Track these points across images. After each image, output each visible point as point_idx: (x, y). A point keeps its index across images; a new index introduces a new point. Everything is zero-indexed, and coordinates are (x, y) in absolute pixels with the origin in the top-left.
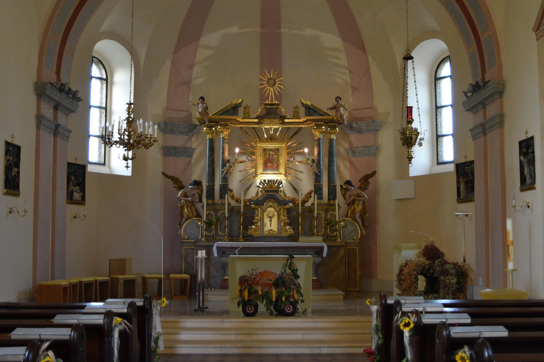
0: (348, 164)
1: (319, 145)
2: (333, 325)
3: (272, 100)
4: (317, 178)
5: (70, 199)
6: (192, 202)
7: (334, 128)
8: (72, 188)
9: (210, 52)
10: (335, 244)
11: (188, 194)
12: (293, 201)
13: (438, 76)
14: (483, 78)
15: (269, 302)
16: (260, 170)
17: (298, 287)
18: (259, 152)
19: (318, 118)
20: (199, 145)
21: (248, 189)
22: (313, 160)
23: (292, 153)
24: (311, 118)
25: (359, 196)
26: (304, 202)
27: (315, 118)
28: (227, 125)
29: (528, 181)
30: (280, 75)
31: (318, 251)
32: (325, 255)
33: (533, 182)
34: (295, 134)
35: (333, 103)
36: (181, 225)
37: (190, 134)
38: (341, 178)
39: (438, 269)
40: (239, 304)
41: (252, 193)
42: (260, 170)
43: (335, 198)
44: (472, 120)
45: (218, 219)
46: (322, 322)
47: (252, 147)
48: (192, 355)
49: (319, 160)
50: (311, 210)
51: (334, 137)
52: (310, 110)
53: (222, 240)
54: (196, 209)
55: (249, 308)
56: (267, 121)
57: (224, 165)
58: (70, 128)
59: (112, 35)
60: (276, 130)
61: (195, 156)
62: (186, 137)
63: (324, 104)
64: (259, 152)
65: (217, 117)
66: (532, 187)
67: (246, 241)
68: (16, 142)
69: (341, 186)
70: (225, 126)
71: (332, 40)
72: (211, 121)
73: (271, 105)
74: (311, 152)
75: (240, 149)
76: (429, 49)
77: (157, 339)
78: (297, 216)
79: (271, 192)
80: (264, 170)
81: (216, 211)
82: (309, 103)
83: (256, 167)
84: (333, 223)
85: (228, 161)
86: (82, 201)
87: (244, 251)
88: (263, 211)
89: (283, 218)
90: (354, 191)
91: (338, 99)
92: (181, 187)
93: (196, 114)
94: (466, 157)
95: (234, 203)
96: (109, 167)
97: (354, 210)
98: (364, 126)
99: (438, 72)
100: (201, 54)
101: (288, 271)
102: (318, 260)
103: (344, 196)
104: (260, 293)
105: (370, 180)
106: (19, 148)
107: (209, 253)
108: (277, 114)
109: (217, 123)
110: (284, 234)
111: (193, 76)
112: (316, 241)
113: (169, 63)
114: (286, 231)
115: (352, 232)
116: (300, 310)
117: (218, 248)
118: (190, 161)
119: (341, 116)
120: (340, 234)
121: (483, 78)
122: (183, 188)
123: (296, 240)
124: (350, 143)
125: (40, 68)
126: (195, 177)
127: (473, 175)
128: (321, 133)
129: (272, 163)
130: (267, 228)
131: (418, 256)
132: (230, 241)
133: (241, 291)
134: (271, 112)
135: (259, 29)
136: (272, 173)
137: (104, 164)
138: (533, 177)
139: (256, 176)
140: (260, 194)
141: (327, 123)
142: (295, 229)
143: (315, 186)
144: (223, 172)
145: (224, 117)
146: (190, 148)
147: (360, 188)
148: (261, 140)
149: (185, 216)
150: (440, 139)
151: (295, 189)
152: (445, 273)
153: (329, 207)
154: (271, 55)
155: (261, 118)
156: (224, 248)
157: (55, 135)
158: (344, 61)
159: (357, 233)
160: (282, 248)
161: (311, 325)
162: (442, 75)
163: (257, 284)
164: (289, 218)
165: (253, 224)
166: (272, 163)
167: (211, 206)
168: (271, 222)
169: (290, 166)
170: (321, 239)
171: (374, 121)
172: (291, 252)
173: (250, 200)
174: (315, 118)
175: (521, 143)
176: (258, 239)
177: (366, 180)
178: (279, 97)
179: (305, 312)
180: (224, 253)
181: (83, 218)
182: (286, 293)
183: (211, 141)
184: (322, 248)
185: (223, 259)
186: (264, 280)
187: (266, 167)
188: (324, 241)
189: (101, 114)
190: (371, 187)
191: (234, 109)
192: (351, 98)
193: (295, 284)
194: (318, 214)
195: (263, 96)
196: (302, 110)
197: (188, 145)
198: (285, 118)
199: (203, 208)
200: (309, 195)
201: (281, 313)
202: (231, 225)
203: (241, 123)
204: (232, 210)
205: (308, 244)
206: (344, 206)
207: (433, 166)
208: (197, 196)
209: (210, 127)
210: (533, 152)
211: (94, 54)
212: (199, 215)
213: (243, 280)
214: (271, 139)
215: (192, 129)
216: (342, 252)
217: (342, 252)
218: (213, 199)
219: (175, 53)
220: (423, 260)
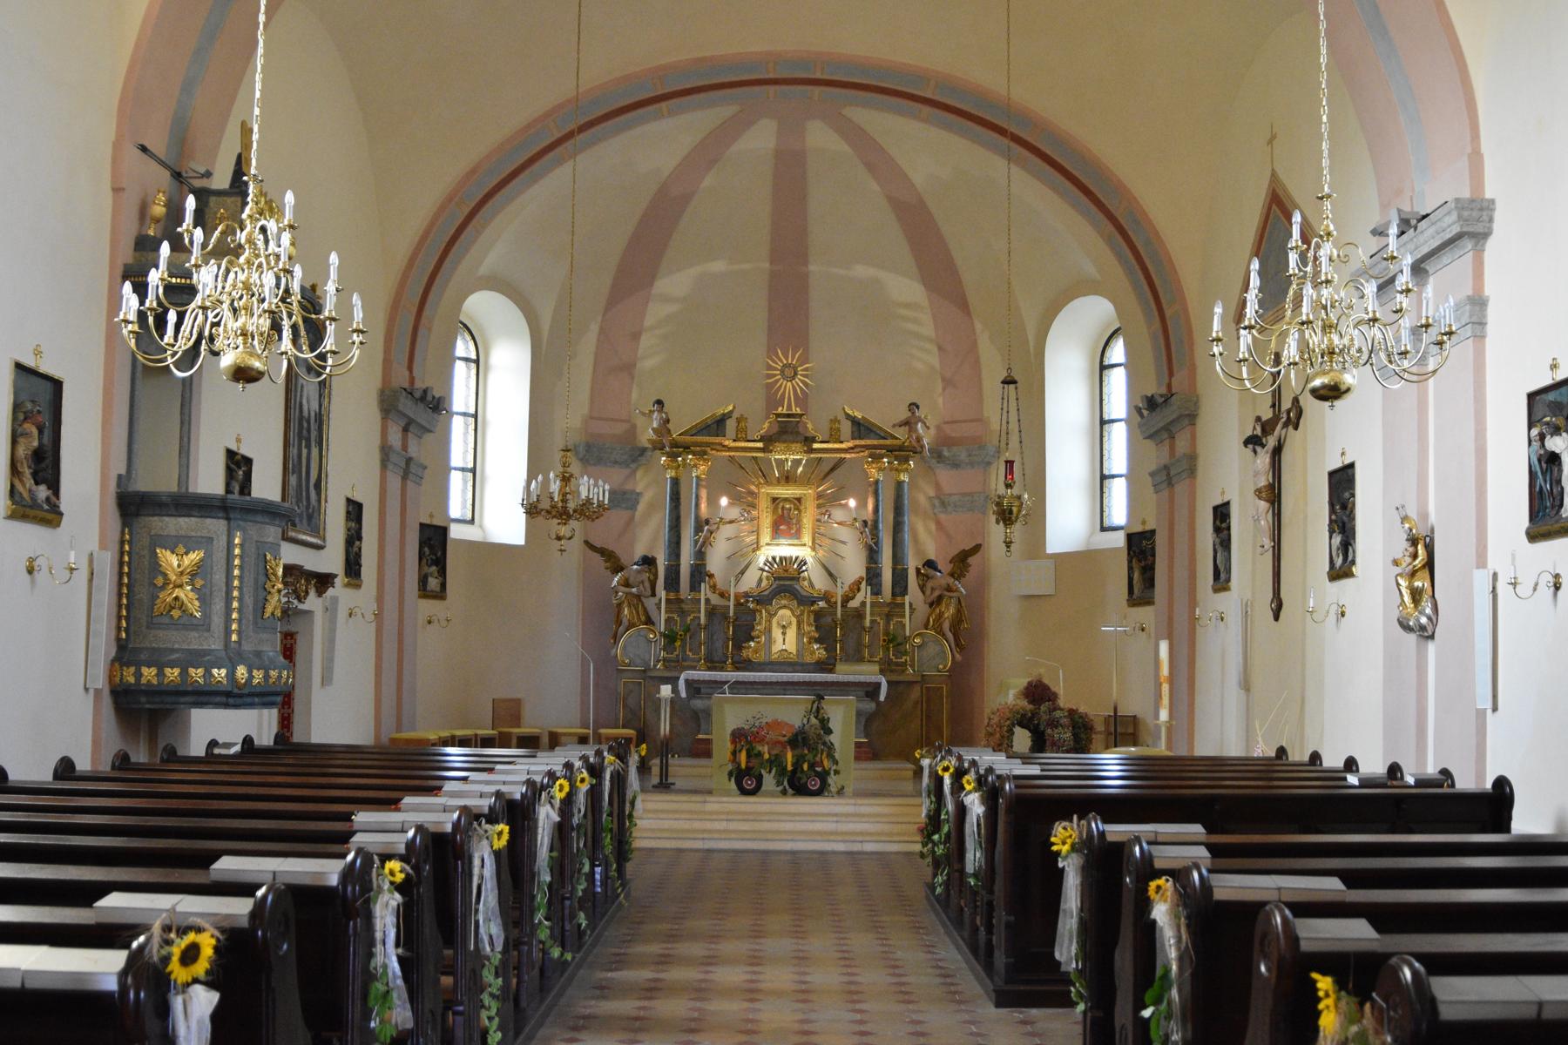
0: (933, 527)
1: (876, 493)
2: (886, 810)
3: (789, 407)
4: (873, 554)
5: (424, 592)
6: (638, 597)
7: (906, 460)
8: (426, 569)
9: (671, 308)
10: (901, 678)
11: (631, 581)
12: (826, 597)
13: (1106, 362)
14: (1169, 386)
15: (782, 771)
16: (766, 537)
17: (830, 748)
18: (764, 504)
19: (875, 442)
20: (651, 485)
21: (742, 572)
22: (865, 522)
23: (827, 503)
24: (862, 442)
25: (949, 589)
26: (847, 599)
27: (869, 442)
28: (705, 453)
29: (1223, 576)
30: (804, 359)
31: (871, 691)
32: (882, 698)
33: (1228, 580)
34: (832, 470)
35: (904, 414)
36: (616, 638)
37: (633, 466)
38: (919, 552)
39: (1045, 717)
40: (730, 774)
41: (749, 582)
42: (766, 537)
43: (904, 592)
44: (1155, 456)
45: (688, 630)
46: (868, 806)
47: (751, 493)
48: (658, 849)
49: (876, 522)
50: (859, 614)
51: (904, 477)
52: (861, 428)
53: (694, 668)
54: (645, 609)
55: (746, 781)
56: (780, 446)
57: (698, 529)
58: (426, 463)
59: (496, 283)
60: (797, 463)
61: (641, 507)
62: (626, 471)
63: (886, 415)
64: (764, 504)
65: (688, 439)
66: (1225, 588)
67: (738, 669)
68: (358, 498)
69: (918, 570)
70: (701, 455)
71: (906, 289)
72: (675, 445)
73: (789, 416)
74: (862, 504)
75: (730, 497)
76: (1090, 314)
77: (634, 798)
78: (833, 625)
79: (786, 580)
80: (773, 538)
81: (683, 613)
82: (859, 415)
83: (758, 533)
84: (900, 640)
85: (707, 522)
86: (441, 594)
87: (738, 686)
88: (771, 616)
89: (807, 628)
90: (941, 579)
91: (914, 406)
92: (618, 568)
93: (647, 435)
94: (1144, 523)
95: (715, 600)
96: (481, 526)
97: (941, 615)
98: (963, 456)
99: (1107, 354)
100: (656, 312)
101: (814, 721)
102: (870, 706)
103: (922, 588)
104: (767, 756)
105: (971, 560)
106: (248, 462)
107: (675, 690)
108: (798, 433)
109: (687, 448)
110: (808, 659)
111: (640, 352)
112: (868, 672)
113: (594, 328)
114: (813, 652)
115: (935, 656)
116: (833, 789)
117: (687, 681)
118: (632, 518)
119: (919, 440)
120: (913, 660)
121: (1169, 386)
122: (622, 569)
123: (831, 671)
124: (938, 486)
125: (387, 363)
126: (640, 551)
127: (1154, 555)
128: (880, 469)
129: (789, 525)
130: (778, 646)
131: (1016, 697)
132: (709, 669)
133: (734, 753)
134: (788, 431)
135: (767, 265)
136: (785, 542)
137: (472, 521)
138: (1228, 571)
139: (758, 548)
140: (764, 583)
141: (891, 450)
142: (830, 649)
143: (868, 569)
144: (696, 542)
145: (699, 439)
146: (633, 492)
147: (952, 575)
148: (767, 479)
149: (625, 621)
150: (1106, 482)
151: (831, 574)
152: (1054, 724)
153: (893, 610)
154: (789, 313)
155: (769, 441)
156: (698, 681)
157: (405, 478)
158: (928, 330)
159: (945, 658)
160: (798, 683)
161: (850, 809)
162: (1113, 362)
163: (762, 741)
164: (818, 628)
165: (752, 639)
166: (789, 525)
167: (675, 604)
168: (784, 635)
169: (822, 530)
170: (876, 668)
171: (982, 447)
172: (819, 691)
173: (746, 595)
174: (869, 442)
175: (1215, 509)
176: (761, 667)
177: (962, 561)
178: (802, 400)
179: (841, 792)
180: (698, 691)
181: (444, 623)
182: (810, 757)
183: (675, 482)
184: (878, 685)
185: (698, 703)
186: (772, 736)
187: (776, 532)
188: (882, 672)
189: (467, 425)
190: (971, 575)
191: (717, 425)
192: (940, 400)
193: (824, 744)
194: (872, 622)
195: (773, 400)
196: (846, 427)
197: (628, 487)
198: (814, 440)
199: (659, 608)
200: (856, 587)
201: (800, 790)
202: (710, 638)
203: (730, 449)
204: (712, 612)
205: (851, 678)
206: (922, 609)
207: (1092, 534)
208: (647, 584)
209: (673, 456)
210: (1229, 528)
211: (462, 318)
212: (649, 621)
213: (738, 735)
214: (788, 479)
215: (636, 455)
216: (915, 693)
217: (915, 693)
218: (677, 591)
219: (607, 310)
220: (1024, 703)
